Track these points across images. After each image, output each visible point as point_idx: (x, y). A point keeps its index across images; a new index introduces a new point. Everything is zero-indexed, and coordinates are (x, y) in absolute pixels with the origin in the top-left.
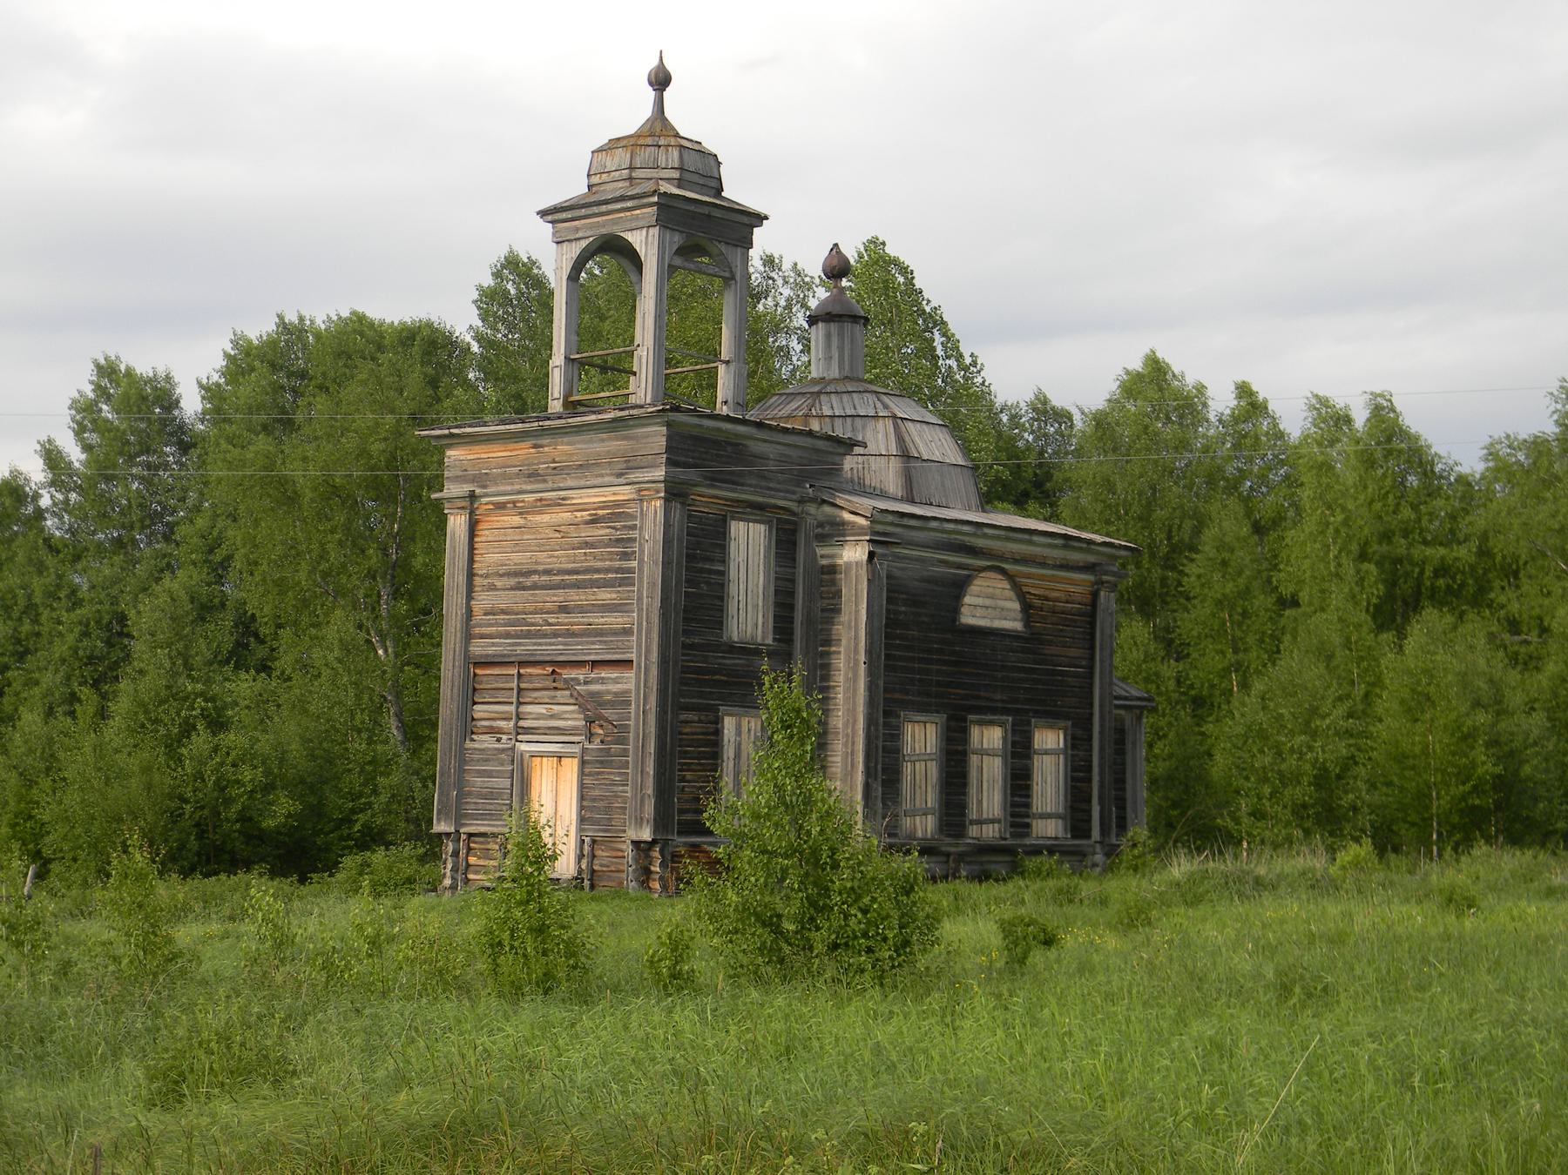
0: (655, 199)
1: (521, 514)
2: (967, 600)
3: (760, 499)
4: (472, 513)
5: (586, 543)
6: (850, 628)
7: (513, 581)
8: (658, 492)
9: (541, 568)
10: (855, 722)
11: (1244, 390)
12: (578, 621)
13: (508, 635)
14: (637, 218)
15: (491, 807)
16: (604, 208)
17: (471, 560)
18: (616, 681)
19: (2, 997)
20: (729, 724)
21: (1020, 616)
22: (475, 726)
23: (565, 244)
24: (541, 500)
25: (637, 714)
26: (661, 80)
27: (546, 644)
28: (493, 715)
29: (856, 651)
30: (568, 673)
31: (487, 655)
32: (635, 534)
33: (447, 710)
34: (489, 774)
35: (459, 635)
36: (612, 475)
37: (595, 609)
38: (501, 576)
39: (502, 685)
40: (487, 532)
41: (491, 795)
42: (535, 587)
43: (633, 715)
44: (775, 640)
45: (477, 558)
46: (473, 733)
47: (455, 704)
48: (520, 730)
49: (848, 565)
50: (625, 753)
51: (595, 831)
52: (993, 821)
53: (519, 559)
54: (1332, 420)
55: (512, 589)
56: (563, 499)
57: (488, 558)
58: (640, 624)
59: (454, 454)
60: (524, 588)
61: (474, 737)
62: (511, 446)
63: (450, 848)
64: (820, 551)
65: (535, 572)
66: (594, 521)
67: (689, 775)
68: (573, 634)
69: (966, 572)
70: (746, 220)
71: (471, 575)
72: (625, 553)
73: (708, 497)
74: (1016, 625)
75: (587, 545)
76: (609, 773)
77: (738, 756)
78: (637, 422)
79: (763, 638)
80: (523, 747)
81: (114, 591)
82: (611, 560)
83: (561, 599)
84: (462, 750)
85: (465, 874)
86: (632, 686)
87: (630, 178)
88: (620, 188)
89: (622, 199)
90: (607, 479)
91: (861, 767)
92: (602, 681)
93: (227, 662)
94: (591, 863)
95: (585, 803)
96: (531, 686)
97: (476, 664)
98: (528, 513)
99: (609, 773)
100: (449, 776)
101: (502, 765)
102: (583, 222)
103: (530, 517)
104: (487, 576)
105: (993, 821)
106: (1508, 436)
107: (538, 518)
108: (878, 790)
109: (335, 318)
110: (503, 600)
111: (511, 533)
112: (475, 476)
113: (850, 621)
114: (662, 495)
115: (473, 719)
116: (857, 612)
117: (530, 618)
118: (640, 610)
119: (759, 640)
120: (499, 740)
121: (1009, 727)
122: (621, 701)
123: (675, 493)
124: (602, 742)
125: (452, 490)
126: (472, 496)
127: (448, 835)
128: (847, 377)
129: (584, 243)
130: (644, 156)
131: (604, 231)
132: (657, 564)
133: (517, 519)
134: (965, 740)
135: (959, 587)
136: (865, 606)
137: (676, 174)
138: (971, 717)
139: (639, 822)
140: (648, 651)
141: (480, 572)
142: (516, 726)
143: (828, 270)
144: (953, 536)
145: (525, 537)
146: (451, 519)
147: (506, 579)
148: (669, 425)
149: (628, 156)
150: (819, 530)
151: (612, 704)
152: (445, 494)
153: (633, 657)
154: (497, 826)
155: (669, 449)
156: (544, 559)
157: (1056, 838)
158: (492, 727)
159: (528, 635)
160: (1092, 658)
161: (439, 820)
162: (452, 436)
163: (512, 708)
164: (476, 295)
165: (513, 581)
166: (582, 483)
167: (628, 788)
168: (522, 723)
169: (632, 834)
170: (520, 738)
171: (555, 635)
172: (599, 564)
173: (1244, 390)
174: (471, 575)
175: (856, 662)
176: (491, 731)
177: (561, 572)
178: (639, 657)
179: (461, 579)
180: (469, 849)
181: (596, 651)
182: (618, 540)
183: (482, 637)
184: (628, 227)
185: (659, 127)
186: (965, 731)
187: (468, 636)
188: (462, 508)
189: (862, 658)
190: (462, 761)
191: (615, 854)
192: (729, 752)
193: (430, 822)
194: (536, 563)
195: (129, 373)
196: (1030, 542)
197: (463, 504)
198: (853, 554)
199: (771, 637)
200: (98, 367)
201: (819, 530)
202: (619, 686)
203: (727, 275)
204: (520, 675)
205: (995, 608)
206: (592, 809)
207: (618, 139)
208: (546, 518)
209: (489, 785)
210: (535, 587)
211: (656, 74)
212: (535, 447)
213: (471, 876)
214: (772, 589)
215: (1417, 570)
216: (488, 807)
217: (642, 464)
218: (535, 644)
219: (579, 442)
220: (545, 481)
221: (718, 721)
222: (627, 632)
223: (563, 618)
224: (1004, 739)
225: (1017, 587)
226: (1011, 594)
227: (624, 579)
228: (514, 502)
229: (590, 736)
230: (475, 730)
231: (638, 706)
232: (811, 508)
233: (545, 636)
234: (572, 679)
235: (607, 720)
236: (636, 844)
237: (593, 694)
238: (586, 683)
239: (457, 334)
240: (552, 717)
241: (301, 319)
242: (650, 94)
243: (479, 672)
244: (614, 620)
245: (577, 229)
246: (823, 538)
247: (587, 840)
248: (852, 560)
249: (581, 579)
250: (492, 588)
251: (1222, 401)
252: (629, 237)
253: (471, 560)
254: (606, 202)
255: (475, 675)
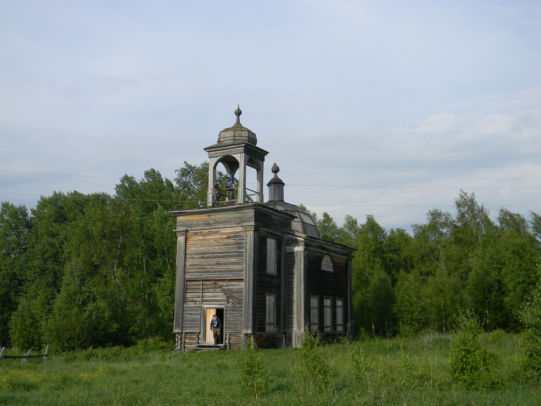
0: (244, 145)
1: (203, 236)
2: (323, 263)
3: (274, 232)
4: (186, 236)
5: (226, 244)
6: (298, 270)
7: (200, 256)
8: (252, 229)
9: (210, 252)
10: (301, 297)
11: (326, 215)
12: (223, 268)
13: (199, 272)
14: (237, 150)
15: (194, 324)
16: (226, 147)
17: (186, 250)
18: (237, 285)
19: (296, 405)
20: (267, 297)
21: (332, 267)
22: (187, 300)
23: (212, 158)
24: (210, 232)
25: (246, 295)
26: (239, 113)
27: (212, 275)
28: (193, 296)
29: (300, 277)
30: (220, 283)
31: (191, 278)
32: (242, 241)
33: (178, 294)
34: (193, 314)
35: (182, 272)
36: (235, 224)
37: (229, 264)
38: (196, 254)
39: (196, 287)
40: (191, 241)
41: (193, 320)
42: (208, 257)
43: (244, 295)
44: (277, 273)
45: (187, 249)
46: (186, 302)
47: (181, 293)
48: (203, 301)
49: (297, 252)
50: (241, 307)
51: (231, 331)
52: (329, 327)
53: (202, 249)
54: (352, 223)
55: (200, 258)
56: (218, 231)
57: (191, 249)
58: (246, 268)
59: (179, 218)
60: (204, 258)
61: (187, 303)
62: (200, 216)
63: (180, 337)
64: (287, 248)
65: (208, 253)
66: (228, 238)
67: (259, 313)
68: (222, 272)
69: (321, 255)
70: (264, 153)
71: (186, 254)
72: (240, 247)
73: (263, 230)
74: (331, 270)
75: (226, 245)
76: (236, 313)
77: (269, 308)
78: (238, 209)
79: (274, 273)
80: (205, 306)
81: (12, 266)
82: (235, 249)
83: (217, 261)
84: (183, 307)
85: (184, 345)
86: (243, 287)
87: (234, 139)
88: (231, 142)
89: (233, 145)
90: (234, 225)
91: (303, 311)
92: (233, 285)
93: (51, 286)
94: (229, 341)
95: (227, 323)
96: (207, 287)
97: (187, 281)
98: (205, 235)
99: (236, 313)
100: (179, 315)
101: (197, 311)
102: (219, 151)
103: (206, 237)
104: (191, 255)
105: (329, 327)
106: (416, 225)
107: (209, 237)
108: (307, 316)
109: (70, 193)
110: (197, 262)
111: (199, 242)
112: (187, 225)
113: (298, 268)
114: (253, 229)
115: (186, 298)
116: (300, 265)
117: (206, 267)
118: (246, 264)
119: (274, 274)
120: (196, 304)
121: (332, 299)
122: (240, 291)
123: (256, 230)
124: (233, 304)
125: (179, 229)
126: (187, 231)
127: (178, 333)
128: (280, 200)
129: (220, 157)
130: (237, 133)
131: (226, 154)
132: (252, 250)
133: (201, 237)
134: (323, 303)
135: (321, 259)
136: (303, 263)
137: (247, 139)
138: (324, 297)
139: (247, 328)
140: (249, 276)
141: (188, 253)
142: (202, 299)
143: (274, 170)
144: (321, 244)
145: (204, 243)
146: (179, 238)
147: (198, 255)
148: (254, 209)
149: (233, 133)
150: (287, 242)
151: (236, 292)
152: (177, 230)
153: (244, 278)
154: (196, 330)
155: (255, 216)
156: (211, 249)
157: (341, 332)
158: (193, 300)
159: (206, 272)
160: (347, 280)
161: (175, 329)
162: (181, 213)
163: (201, 294)
164: (115, 187)
165: (200, 256)
166: (225, 226)
167: (243, 318)
168: (203, 299)
169: (245, 331)
170: (203, 303)
171: (215, 272)
172: (230, 250)
173: (326, 215)
174: (186, 254)
175: (301, 280)
176: (193, 301)
177: (217, 253)
178: (246, 278)
179: (183, 255)
180: (185, 337)
181: (230, 276)
182: (237, 243)
183: (189, 273)
184: (234, 153)
185: (238, 126)
186: (323, 301)
187: (185, 273)
188: (183, 234)
189: (303, 279)
190: (183, 311)
191: (237, 338)
192: (267, 307)
193: (172, 330)
194: (208, 250)
195: (12, 206)
196: (336, 247)
197: (183, 233)
198: (299, 249)
199: (276, 273)
200: (3, 204)
201: (287, 242)
202: (239, 287)
203: (258, 168)
204: (203, 284)
205: (328, 265)
206: (229, 324)
207: (228, 128)
208: (212, 237)
209: (193, 317)
210: (208, 257)
211: (238, 111)
212: (208, 216)
213: (186, 346)
214: (276, 259)
215: (385, 260)
216: (192, 324)
217: (246, 221)
218: (208, 275)
219: (224, 214)
220: (212, 226)
221: (265, 297)
222: (241, 271)
223: (218, 267)
224: (331, 303)
225: (332, 260)
226: (330, 261)
227: (240, 255)
228: (201, 232)
229: (228, 302)
230: (187, 301)
231: (246, 293)
232: (285, 235)
233: (212, 272)
234: (222, 285)
235: (234, 297)
236: (247, 335)
237: (229, 289)
238: (227, 286)
239: (111, 196)
240: (214, 296)
241: (60, 193)
242: (235, 117)
243: (188, 283)
244: (237, 267)
245: (217, 154)
246: (288, 244)
247: (228, 334)
248: (298, 250)
249: (225, 255)
250: (193, 258)
251: (320, 217)
252: (234, 156)
253: (186, 250)
254: (222, 147)
255: (187, 284)
